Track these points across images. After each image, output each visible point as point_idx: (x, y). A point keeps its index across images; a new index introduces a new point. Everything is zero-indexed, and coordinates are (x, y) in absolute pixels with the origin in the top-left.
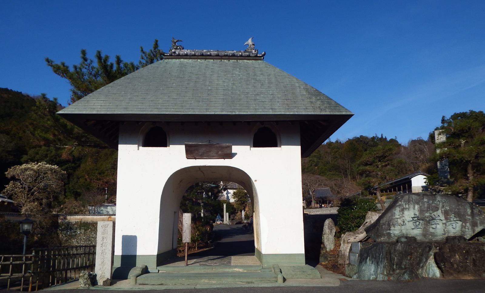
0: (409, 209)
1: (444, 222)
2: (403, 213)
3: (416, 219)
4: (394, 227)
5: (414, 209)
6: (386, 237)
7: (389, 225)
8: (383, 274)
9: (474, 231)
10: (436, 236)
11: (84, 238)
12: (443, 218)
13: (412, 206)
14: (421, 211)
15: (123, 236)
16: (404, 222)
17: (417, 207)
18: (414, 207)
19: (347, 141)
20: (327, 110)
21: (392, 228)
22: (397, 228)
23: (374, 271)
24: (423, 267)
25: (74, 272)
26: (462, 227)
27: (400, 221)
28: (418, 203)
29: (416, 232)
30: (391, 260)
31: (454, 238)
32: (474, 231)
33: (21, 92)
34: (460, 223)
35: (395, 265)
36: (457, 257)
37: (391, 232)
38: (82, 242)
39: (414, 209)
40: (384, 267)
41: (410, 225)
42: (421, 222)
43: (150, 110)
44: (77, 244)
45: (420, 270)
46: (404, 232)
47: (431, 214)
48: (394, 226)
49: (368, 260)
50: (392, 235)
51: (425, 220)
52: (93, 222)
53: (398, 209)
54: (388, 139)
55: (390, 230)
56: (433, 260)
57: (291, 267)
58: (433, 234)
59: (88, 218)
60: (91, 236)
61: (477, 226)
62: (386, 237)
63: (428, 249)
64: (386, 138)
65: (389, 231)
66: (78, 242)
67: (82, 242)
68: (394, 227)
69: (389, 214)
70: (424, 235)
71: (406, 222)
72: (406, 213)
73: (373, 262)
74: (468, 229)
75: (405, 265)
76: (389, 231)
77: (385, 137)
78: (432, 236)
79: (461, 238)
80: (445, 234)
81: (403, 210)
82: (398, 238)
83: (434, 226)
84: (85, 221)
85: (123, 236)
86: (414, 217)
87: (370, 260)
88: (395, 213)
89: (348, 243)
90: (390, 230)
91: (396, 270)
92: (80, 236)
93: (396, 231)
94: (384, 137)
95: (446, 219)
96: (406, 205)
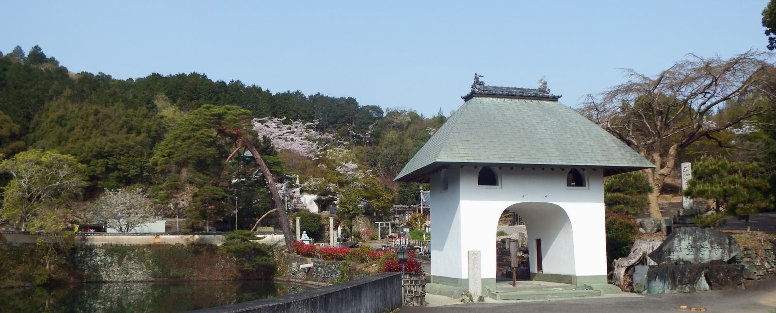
1: (710, 249)
2: (680, 243)
3: (690, 247)
4: (673, 253)
5: (689, 239)
9: (730, 256)
10: (704, 260)
11: (119, 269)
12: (709, 246)
13: (687, 237)
14: (695, 241)
17: (691, 238)
18: (689, 238)
19: (142, 78)
20: (637, 162)
21: (672, 254)
22: (676, 254)
24: (696, 283)
26: (723, 253)
27: (678, 248)
28: (692, 235)
29: (690, 257)
31: (717, 261)
32: (730, 256)
34: (721, 250)
36: (721, 274)
37: (671, 257)
38: (116, 276)
39: (689, 239)
40: (669, 284)
41: (685, 252)
42: (693, 249)
43: (568, 161)
44: (107, 279)
47: (701, 243)
48: (673, 252)
49: (657, 279)
50: (672, 260)
51: (696, 248)
52: (130, 245)
55: (670, 255)
56: (704, 278)
58: (701, 259)
59: (123, 239)
60: (129, 265)
61: (732, 253)
63: (701, 269)
65: (669, 257)
66: (108, 275)
67: (116, 276)
68: (673, 253)
69: (670, 243)
70: (695, 259)
71: (682, 249)
72: (683, 242)
74: (726, 255)
76: (669, 257)
78: (701, 260)
79: (721, 261)
80: (710, 259)
81: (680, 240)
83: (702, 253)
84: (118, 244)
85: (480, 251)
89: (622, 266)
92: (112, 266)
93: (674, 256)
95: (712, 247)
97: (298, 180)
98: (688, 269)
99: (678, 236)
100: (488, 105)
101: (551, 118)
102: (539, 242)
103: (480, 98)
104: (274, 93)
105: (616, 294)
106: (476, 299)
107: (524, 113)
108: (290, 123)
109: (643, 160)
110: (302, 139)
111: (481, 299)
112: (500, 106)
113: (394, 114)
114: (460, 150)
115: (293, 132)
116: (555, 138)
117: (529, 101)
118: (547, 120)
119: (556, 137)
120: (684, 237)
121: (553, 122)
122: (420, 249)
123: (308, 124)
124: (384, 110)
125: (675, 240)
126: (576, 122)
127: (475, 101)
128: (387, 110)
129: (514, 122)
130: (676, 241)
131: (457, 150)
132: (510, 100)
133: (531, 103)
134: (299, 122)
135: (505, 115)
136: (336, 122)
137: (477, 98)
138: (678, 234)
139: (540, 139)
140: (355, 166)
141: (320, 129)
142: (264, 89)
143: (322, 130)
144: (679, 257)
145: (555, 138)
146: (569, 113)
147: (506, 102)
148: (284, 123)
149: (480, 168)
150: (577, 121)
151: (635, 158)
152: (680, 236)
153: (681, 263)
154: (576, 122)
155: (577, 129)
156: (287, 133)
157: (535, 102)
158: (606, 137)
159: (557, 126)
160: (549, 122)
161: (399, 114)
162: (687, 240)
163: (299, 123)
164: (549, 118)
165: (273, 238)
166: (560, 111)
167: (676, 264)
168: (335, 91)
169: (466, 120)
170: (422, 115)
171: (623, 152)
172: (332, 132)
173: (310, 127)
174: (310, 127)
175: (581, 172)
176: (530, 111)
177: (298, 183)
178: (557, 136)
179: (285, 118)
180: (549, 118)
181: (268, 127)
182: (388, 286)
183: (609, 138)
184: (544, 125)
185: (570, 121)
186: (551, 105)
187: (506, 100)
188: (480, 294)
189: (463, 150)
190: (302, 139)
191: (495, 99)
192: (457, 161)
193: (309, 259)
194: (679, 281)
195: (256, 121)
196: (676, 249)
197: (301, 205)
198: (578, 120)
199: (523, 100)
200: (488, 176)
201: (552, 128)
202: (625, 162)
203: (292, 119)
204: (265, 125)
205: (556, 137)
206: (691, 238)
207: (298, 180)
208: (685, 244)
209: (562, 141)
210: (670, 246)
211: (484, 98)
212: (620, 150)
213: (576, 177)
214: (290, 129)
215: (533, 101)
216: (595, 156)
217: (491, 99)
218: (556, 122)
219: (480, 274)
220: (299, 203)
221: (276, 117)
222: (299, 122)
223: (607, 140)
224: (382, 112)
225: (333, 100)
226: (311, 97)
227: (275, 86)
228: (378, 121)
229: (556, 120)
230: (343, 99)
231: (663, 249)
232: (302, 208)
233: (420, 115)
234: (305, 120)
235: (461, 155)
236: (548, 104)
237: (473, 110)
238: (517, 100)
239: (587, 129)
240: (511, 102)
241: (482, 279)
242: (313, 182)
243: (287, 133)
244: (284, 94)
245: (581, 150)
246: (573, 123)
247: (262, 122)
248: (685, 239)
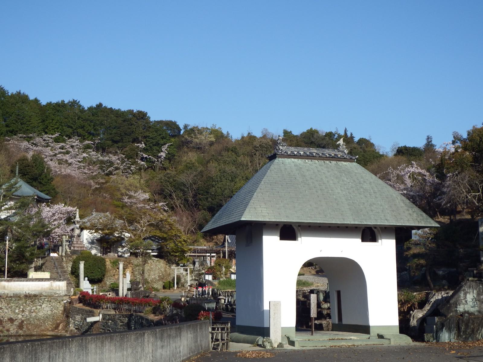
0: (470, 293)
2: (466, 296)
5: (473, 293)
6: (454, 313)
7: (457, 305)
8: (454, 338)
15: (280, 302)
16: (466, 302)
21: (458, 307)
22: (462, 306)
23: (448, 337)
25: (187, 334)
27: (464, 301)
28: (476, 289)
30: (459, 329)
33: (101, 105)
35: (462, 333)
37: (458, 309)
39: (473, 293)
40: (455, 334)
45: (478, 335)
46: (466, 309)
50: (458, 311)
53: (463, 292)
54: (356, 139)
57: (391, 335)
62: (454, 313)
64: (352, 137)
65: (456, 309)
69: (456, 297)
72: (468, 295)
73: (447, 331)
75: (469, 332)
76: (456, 309)
77: (351, 134)
82: (463, 314)
85: (280, 302)
86: (473, 299)
87: (445, 329)
88: (460, 296)
90: (457, 308)
91: (463, 336)
93: (461, 309)
94: (349, 135)
96: (468, 290)
97: (77, 216)
98: (470, 321)
99: (464, 290)
100: (289, 165)
101: (347, 179)
102: (339, 293)
103: (283, 159)
104: (44, 102)
105: (406, 340)
106: (275, 345)
107: (323, 174)
108: (64, 141)
109: (428, 220)
110: (79, 162)
111: (280, 345)
112: (301, 166)
113: (192, 131)
114: (263, 209)
115: (68, 153)
116: (350, 198)
117: (328, 162)
118: (343, 181)
119: (351, 197)
120: (469, 291)
121: (349, 183)
122: (225, 300)
123: (87, 142)
124: (181, 127)
125: (461, 293)
126: (370, 183)
127: (278, 161)
128: (186, 127)
129: (313, 183)
130: (462, 295)
131: (260, 209)
132: (310, 160)
133: (330, 164)
134: (74, 141)
135: (305, 176)
136: (121, 140)
137: (280, 159)
138: (464, 288)
139: (336, 199)
140: (147, 196)
141: (101, 148)
142: (32, 98)
143: (104, 150)
144: (464, 309)
145: (350, 198)
146: (364, 174)
147: (307, 163)
148: (57, 140)
149: (280, 227)
150: (370, 182)
151: (422, 218)
152: (466, 289)
153: (466, 315)
154: (370, 183)
155: (370, 190)
156: (60, 153)
157: (334, 162)
158: (397, 198)
159: (352, 187)
160: (345, 183)
161: (200, 131)
162: (471, 293)
163: (75, 141)
164: (345, 179)
165: (51, 286)
166: (356, 171)
167: (461, 315)
168: (121, 101)
169: (269, 180)
170: (228, 134)
171: (411, 212)
172: (116, 152)
173: (88, 147)
174: (88, 147)
175: (375, 230)
176: (328, 172)
177: (78, 219)
178: (352, 196)
179: (57, 135)
180: (345, 179)
181: (35, 144)
182: (199, 330)
183: (399, 198)
184: (340, 186)
185: (365, 182)
186: (348, 165)
187: (307, 161)
188: (279, 341)
189: (266, 209)
190: (79, 162)
191: (296, 160)
192: (260, 220)
193: (97, 311)
194: (463, 332)
195: (20, 137)
196: (462, 302)
197: (80, 246)
198: (372, 181)
199: (323, 161)
200: (288, 232)
201: (347, 189)
202: (411, 222)
203: (66, 137)
204: (33, 143)
205: (351, 197)
206: (475, 292)
207: (77, 216)
208: (470, 297)
209: (356, 201)
210: (456, 299)
211: (286, 159)
212: (408, 210)
213: (369, 234)
214: (62, 148)
215: (331, 162)
216: (385, 216)
217: (293, 159)
218: (352, 183)
219: (280, 323)
220: (79, 243)
221: (46, 133)
222: (74, 141)
223: (397, 201)
224: (179, 130)
225: (117, 113)
226: (90, 109)
227: (46, 93)
228: (173, 140)
229: (352, 181)
230: (131, 112)
231: (451, 302)
232: (82, 249)
233: (225, 132)
234: (83, 138)
235: (263, 214)
236: (346, 165)
237: (275, 171)
238: (316, 161)
239: (380, 189)
240: (311, 163)
241: (282, 328)
242: (96, 217)
243: (60, 153)
244: (57, 104)
245: (372, 211)
246: (367, 184)
247: (29, 139)
248: (470, 292)
